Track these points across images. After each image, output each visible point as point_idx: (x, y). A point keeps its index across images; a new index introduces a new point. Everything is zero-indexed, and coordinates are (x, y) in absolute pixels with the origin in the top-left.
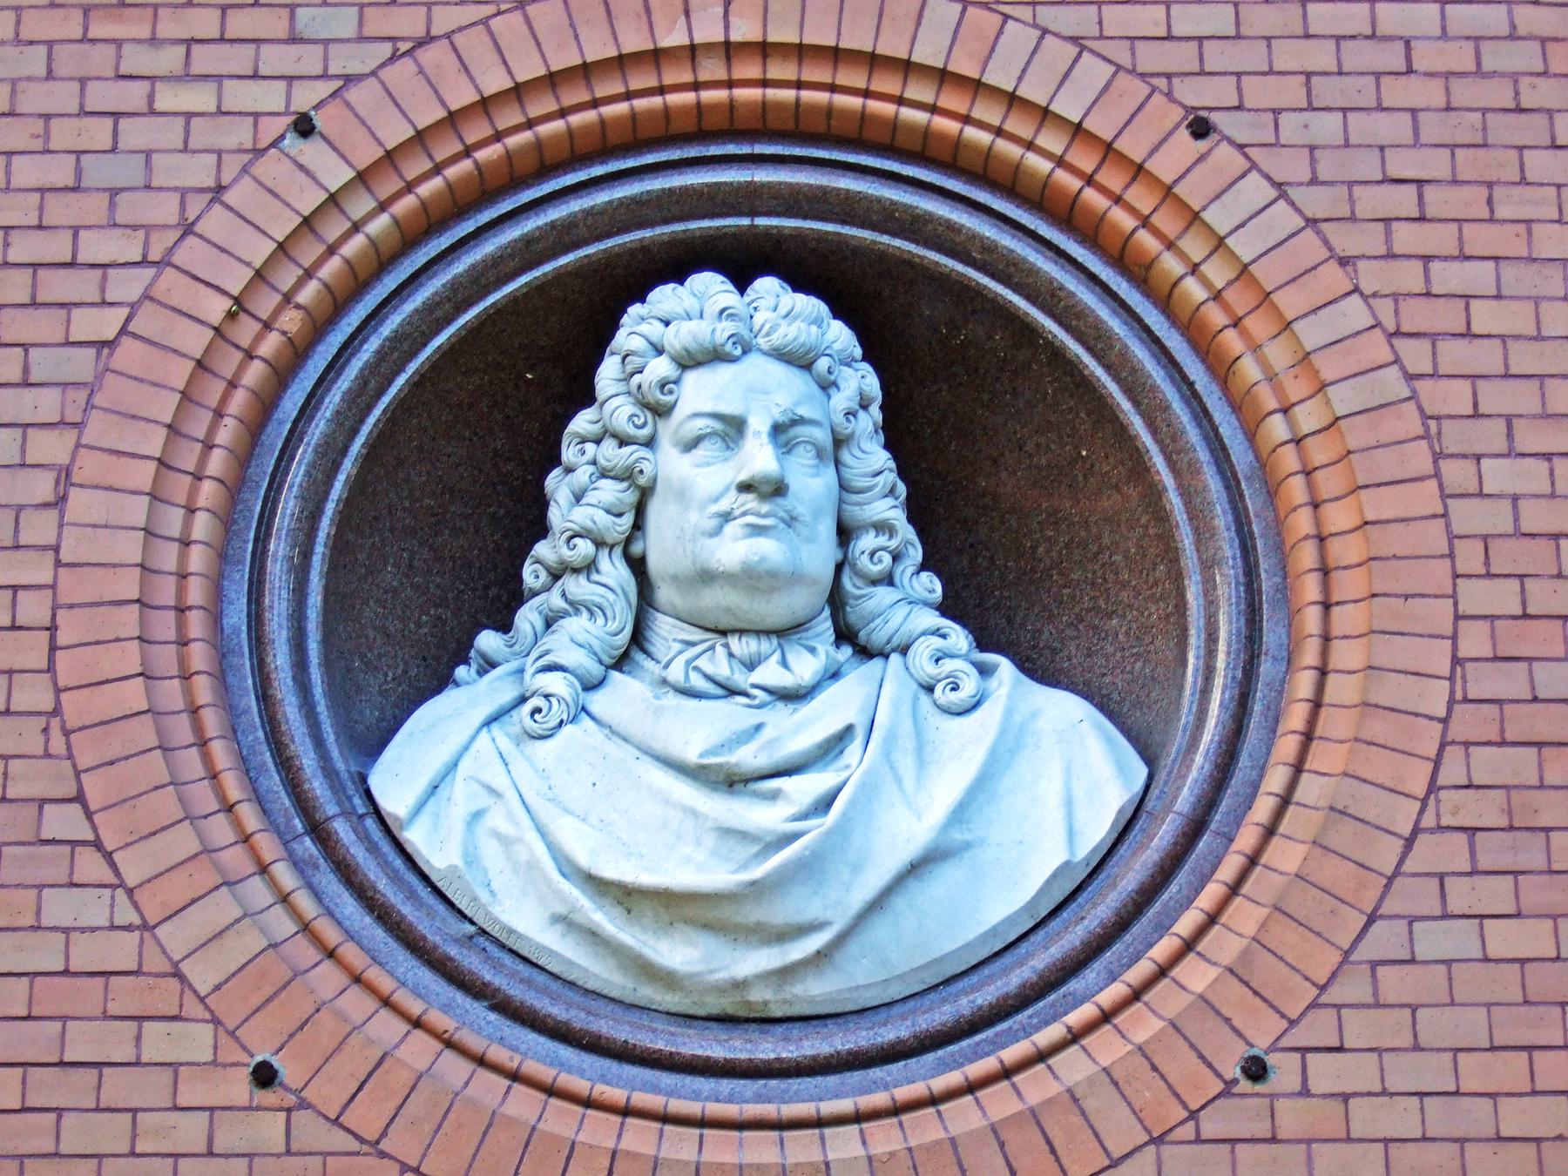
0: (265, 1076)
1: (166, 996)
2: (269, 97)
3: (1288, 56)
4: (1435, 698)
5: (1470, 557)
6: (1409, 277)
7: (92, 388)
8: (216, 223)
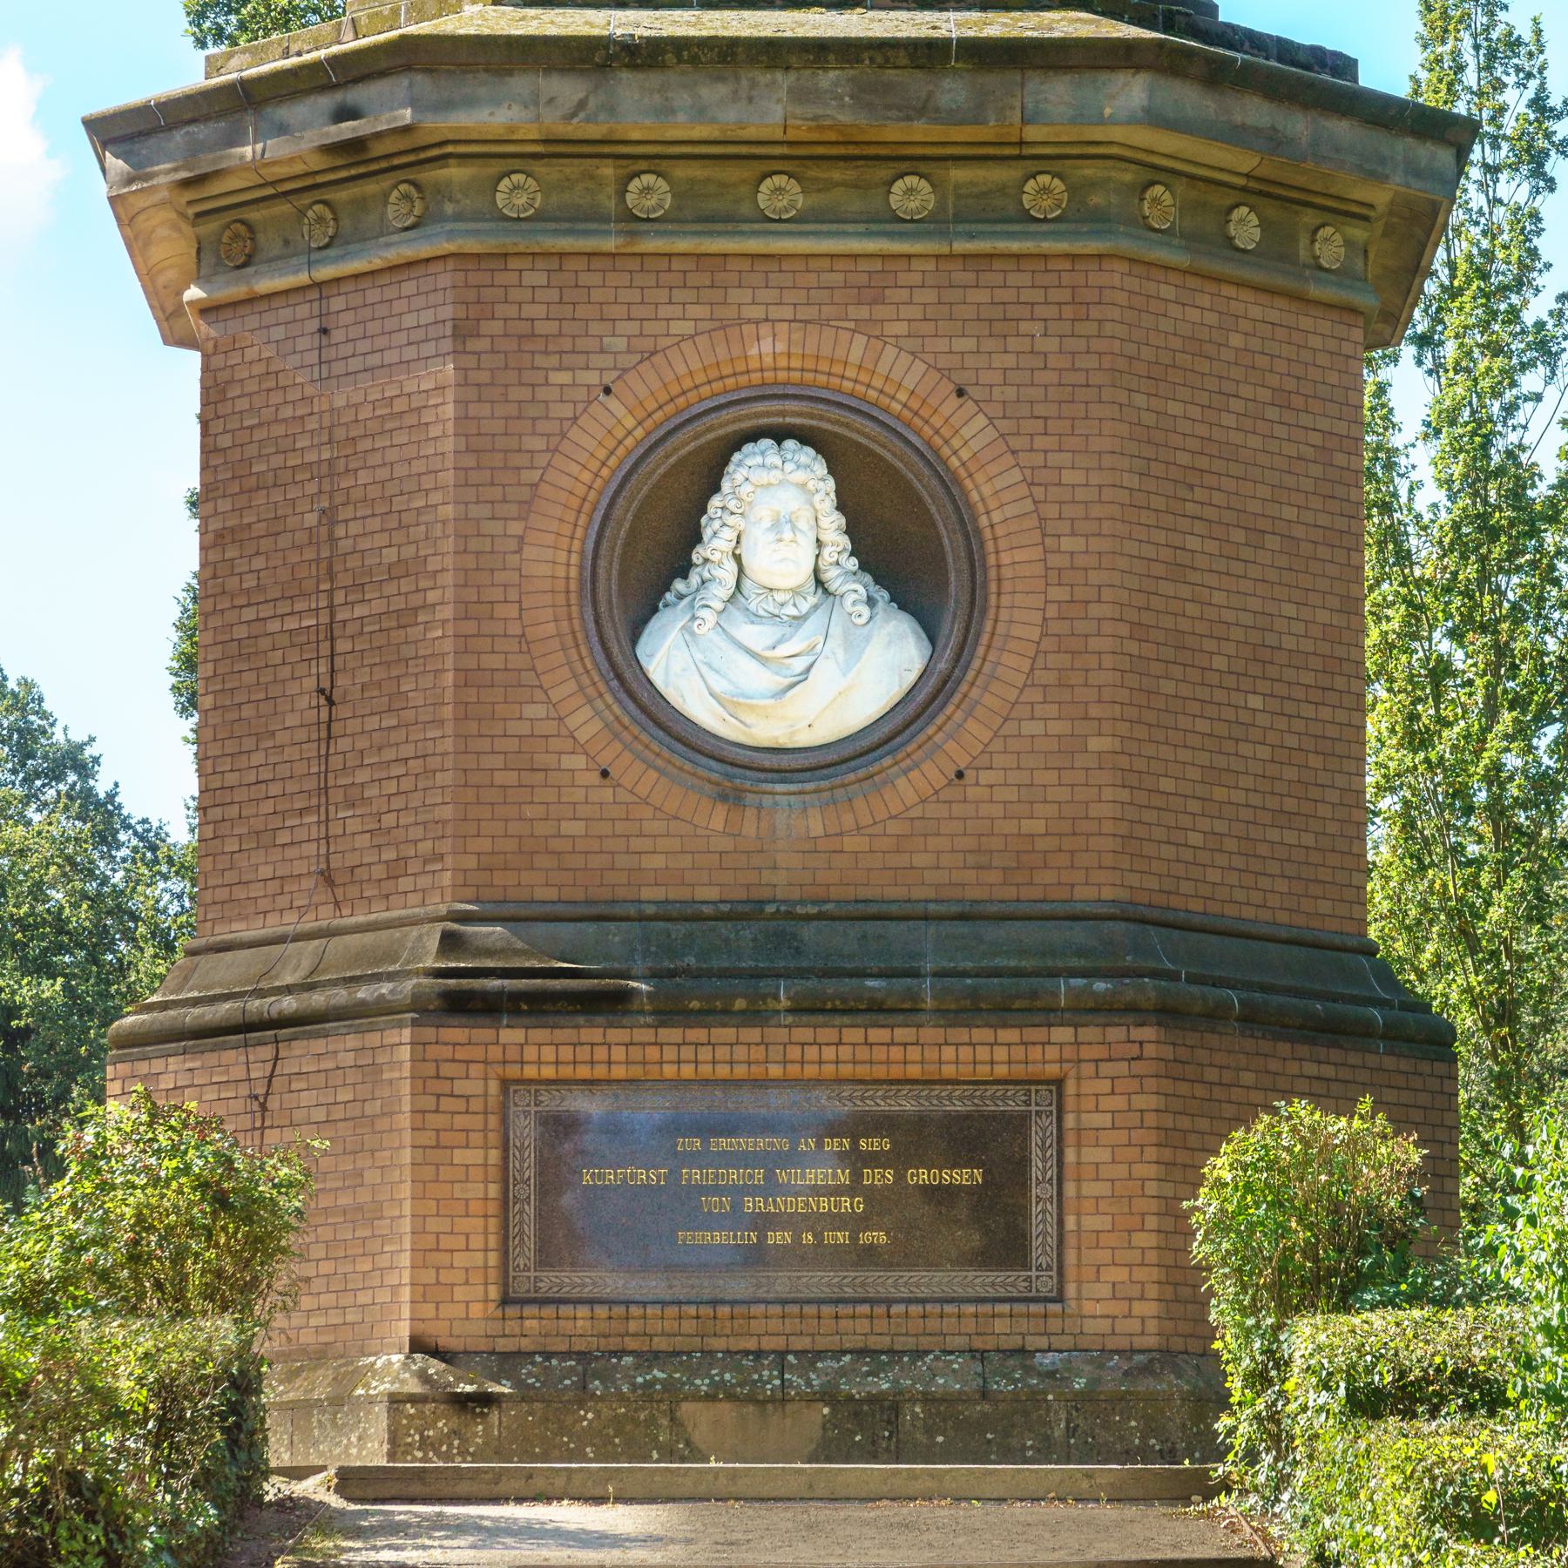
0: (605, 774)
1: (568, 744)
2: (592, 378)
3: (998, 361)
4: (1035, 634)
5: (1053, 575)
6: (1038, 459)
7: (529, 503)
8: (574, 433)
